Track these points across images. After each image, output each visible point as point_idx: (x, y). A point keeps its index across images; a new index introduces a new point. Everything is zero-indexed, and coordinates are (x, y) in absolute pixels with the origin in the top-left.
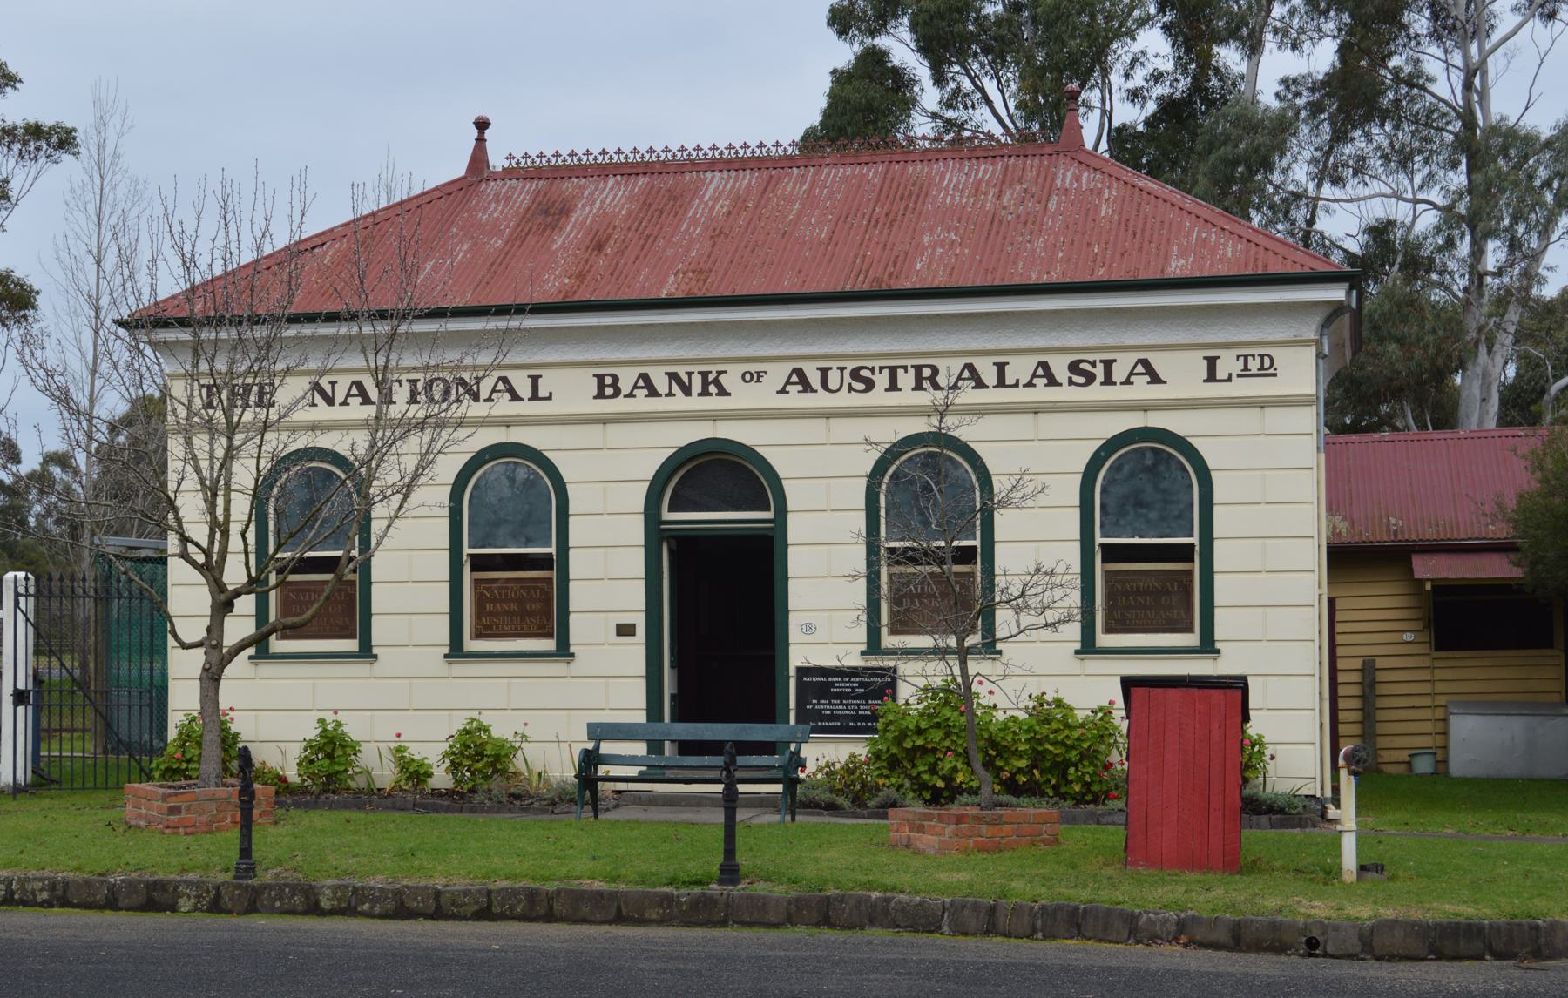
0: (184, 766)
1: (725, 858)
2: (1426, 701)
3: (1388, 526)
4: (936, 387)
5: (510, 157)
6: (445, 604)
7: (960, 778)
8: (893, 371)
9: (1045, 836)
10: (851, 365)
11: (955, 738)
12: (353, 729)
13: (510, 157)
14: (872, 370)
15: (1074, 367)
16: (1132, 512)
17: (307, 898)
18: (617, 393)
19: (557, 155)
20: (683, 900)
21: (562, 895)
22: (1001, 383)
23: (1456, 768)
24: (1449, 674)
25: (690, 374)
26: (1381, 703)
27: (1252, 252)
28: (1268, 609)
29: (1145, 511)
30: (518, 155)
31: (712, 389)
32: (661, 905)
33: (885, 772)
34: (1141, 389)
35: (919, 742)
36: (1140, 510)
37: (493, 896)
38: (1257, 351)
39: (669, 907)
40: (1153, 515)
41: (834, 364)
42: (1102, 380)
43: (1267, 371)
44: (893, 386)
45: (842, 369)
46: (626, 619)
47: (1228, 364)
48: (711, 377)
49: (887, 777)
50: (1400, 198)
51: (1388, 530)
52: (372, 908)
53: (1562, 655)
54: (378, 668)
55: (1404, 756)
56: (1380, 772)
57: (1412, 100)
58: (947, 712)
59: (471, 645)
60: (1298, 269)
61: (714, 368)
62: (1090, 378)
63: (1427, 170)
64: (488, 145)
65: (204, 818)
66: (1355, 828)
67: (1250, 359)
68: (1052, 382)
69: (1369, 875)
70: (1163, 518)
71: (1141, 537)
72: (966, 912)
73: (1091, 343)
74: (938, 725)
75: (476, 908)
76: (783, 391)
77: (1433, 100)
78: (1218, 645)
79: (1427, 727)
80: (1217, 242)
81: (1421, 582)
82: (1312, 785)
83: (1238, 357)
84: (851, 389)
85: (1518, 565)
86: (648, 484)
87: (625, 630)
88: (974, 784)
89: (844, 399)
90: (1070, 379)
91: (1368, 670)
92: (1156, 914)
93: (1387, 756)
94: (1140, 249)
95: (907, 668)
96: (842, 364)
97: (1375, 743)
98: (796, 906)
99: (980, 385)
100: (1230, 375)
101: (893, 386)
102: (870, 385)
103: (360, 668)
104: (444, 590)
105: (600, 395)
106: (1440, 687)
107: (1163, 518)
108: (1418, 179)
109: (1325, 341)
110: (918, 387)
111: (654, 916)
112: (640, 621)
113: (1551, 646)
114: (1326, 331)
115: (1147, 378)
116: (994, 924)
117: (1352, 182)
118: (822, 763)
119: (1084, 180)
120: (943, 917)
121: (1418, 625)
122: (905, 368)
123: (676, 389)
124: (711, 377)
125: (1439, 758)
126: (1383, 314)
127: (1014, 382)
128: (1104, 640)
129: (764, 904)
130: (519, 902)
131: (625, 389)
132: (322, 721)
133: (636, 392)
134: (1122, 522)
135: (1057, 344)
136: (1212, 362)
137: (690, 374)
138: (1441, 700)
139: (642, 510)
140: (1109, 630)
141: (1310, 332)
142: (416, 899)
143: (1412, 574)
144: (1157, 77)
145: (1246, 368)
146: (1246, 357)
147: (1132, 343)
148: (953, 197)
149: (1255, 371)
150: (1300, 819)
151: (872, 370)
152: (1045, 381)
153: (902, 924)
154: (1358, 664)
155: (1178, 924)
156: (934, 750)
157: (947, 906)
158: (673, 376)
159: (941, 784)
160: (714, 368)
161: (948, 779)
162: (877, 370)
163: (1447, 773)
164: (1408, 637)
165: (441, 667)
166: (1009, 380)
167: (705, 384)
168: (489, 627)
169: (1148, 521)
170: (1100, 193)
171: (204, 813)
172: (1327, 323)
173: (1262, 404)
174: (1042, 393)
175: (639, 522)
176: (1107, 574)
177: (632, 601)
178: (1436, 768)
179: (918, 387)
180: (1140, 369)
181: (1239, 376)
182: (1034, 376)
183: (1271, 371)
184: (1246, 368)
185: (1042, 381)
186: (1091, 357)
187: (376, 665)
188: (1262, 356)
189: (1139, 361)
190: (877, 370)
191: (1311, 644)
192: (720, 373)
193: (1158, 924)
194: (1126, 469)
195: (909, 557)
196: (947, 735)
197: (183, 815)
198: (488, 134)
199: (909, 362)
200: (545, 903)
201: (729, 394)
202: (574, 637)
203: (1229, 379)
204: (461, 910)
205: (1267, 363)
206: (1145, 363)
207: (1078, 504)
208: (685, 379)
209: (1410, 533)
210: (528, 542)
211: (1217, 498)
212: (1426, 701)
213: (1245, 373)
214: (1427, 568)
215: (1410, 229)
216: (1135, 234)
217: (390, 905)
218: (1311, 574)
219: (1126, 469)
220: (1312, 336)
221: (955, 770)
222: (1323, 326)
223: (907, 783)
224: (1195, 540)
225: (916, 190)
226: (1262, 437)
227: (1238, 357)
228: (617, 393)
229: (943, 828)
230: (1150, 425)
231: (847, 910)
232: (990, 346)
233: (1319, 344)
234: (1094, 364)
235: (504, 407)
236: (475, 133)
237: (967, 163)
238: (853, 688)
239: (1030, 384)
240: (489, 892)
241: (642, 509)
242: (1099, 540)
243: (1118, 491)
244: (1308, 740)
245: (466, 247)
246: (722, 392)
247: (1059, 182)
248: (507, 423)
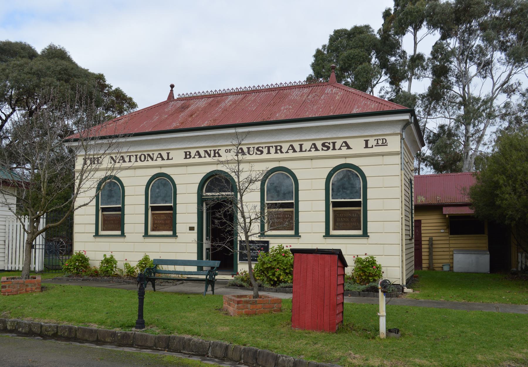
0: (70, 267)
1: (139, 318)
2: (447, 250)
3: (436, 199)
4: (282, 152)
5: (179, 95)
6: (143, 221)
7: (281, 278)
8: (269, 148)
9: (275, 308)
10: (256, 146)
11: (280, 264)
12: (116, 257)
13: (179, 95)
14: (263, 148)
15: (323, 145)
16: (341, 191)
17: (4, 325)
18: (190, 157)
19: (191, 93)
20: (119, 335)
21: (80, 330)
22: (301, 150)
23: (456, 269)
24: (454, 242)
25: (210, 151)
26: (434, 250)
27: (380, 106)
28: (385, 222)
29: (345, 191)
30: (181, 94)
31: (217, 155)
32: (111, 336)
33: (259, 275)
34: (345, 151)
35: (269, 266)
36: (344, 190)
37: (59, 328)
38: (381, 138)
39: (114, 337)
40: (348, 192)
41: (252, 146)
43: (384, 144)
44: (269, 153)
45: (254, 148)
46: (192, 225)
47: (372, 142)
48: (216, 151)
49: (259, 277)
50: (446, 118)
51: (436, 201)
52: (22, 330)
53: (487, 236)
54: (126, 239)
55: (441, 265)
56: (433, 270)
57: (448, 93)
58: (279, 256)
59: (333, 232)
60: (391, 109)
61: (217, 149)
62: (328, 148)
63: (453, 111)
64: (174, 92)
65: (15, 290)
66: (385, 315)
67: (379, 140)
68: (317, 150)
69: (393, 335)
70: (351, 193)
72: (217, 348)
73: (329, 137)
74: (275, 260)
75: (53, 332)
77: (454, 93)
78: (369, 234)
79: (448, 257)
80: (370, 104)
81: (445, 215)
82: (399, 281)
83: (375, 140)
84: (256, 154)
85: (472, 209)
86: (198, 184)
87: (192, 229)
88: (286, 280)
89: (255, 157)
90: (322, 148)
91: (431, 240)
92: (286, 357)
93: (436, 265)
94: (345, 107)
96: (254, 146)
97: (432, 262)
98: (158, 340)
99: (295, 151)
100: (373, 146)
101: (269, 153)
102: (262, 152)
103: (121, 239)
104: (143, 217)
105: (186, 158)
106: (451, 246)
107: (351, 193)
108: (451, 113)
109: (404, 134)
110: (276, 152)
111: (109, 340)
112: (196, 226)
113: (484, 234)
114: (404, 130)
115: (346, 147)
116: (227, 354)
117: (434, 115)
118: (243, 271)
119: (334, 91)
120: (209, 349)
121: (445, 228)
122: (272, 147)
123: (207, 155)
124: (216, 151)
125: (451, 266)
126: (441, 146)
127: (305, 150)
128: (101, 233)
129: (146, 339)
130: (66, 331)
131: (193, 156)
132: (105, 255)
133: (195, 157)
134: (338, 194)
135: (318, 137)
136: (367, 142)
137: (210, 151)
138: (452, 249)
139: (197, 192)
140: (335, 229)
141: (398, 131)
142: (35, 328)
143: (443, 212)
145: (378, 143)
146: (378, 140)
147: (341, 136)
148: (294, 97)
149: (380, 144)
150: (391, 294)
151: (263, 148)
152: (314, 149)
153: (194, 351)
154: (428, 239)
155: (294, 363)
156: (274, 268)
157: (211, 344)
158: (206, 151)
159: (276, 279)
160: (217, 149)
161: (278, 278)
162: (264, 148)
163: (453, 270)
164: (442, 231)
165: (141, 239)
166: (304, 149)
167: (215, 153)
168: (156, 228)
169: (346, 194)
170: (337, 93)
171: (15, 288)
172: (404, 128)
173: (383, 155)
174: (313, 153)
176: (334, 211)
177: (193, 220)
178: (450, 269)
179: (276, 152)
180: (344, 144)
181: (375, 146)
182: (311, 148)
183: (386, 144)
184: (378, 143)
185: (313, 150)
186: (328, 141)
187: (126, 238)
188: (383, 139)
189: (344, 142)
190: (264, 148)
191: (399, 234)
192: (219, 150)
193: (286, 362)
195: (275, 205)
196: (278, 264)
197: (7, 288)
198: (174, 89)
199: (273, 145)
200: (74, 333)
201: (221, 156)
202: (301, 230)
203: (372, 147)
204: (48, 333)
205: (384, 141)
206: (345, 143)
207: (324, 188)
208: (209, 152)
209: (442, 201)
210: (166, 202)
211: (368, 186)
212: (447, 250)
213: (377, 145)
214: (447, 211)
215: (450, 125)
216: (345, 103)
217: (27, 329)
218: (399, 211)
220: (399, 132)
221: (280, 275)
222: (403, 129)
223: (265, 279)
224: (361, 200)
225: (284, 96)
226: (383, 166)
227: (375, 140)
228: (190, 157)
229: (234, 305)
230: (347, 162)
231: (175, 343)
232: (298, 139)
233: (402, 135)
234: (329, 144)
235: (159, 162)
236: (170, 89)
237: (301, 89)
238: (256, 247)
239: (310, 151)
240: (57, 327)
241: (196, 192)
242: (331, 200)
244: (398, 266)
245: (157, 118)
246: (220, 156)
247: (326, 92)
248: (161, 167)
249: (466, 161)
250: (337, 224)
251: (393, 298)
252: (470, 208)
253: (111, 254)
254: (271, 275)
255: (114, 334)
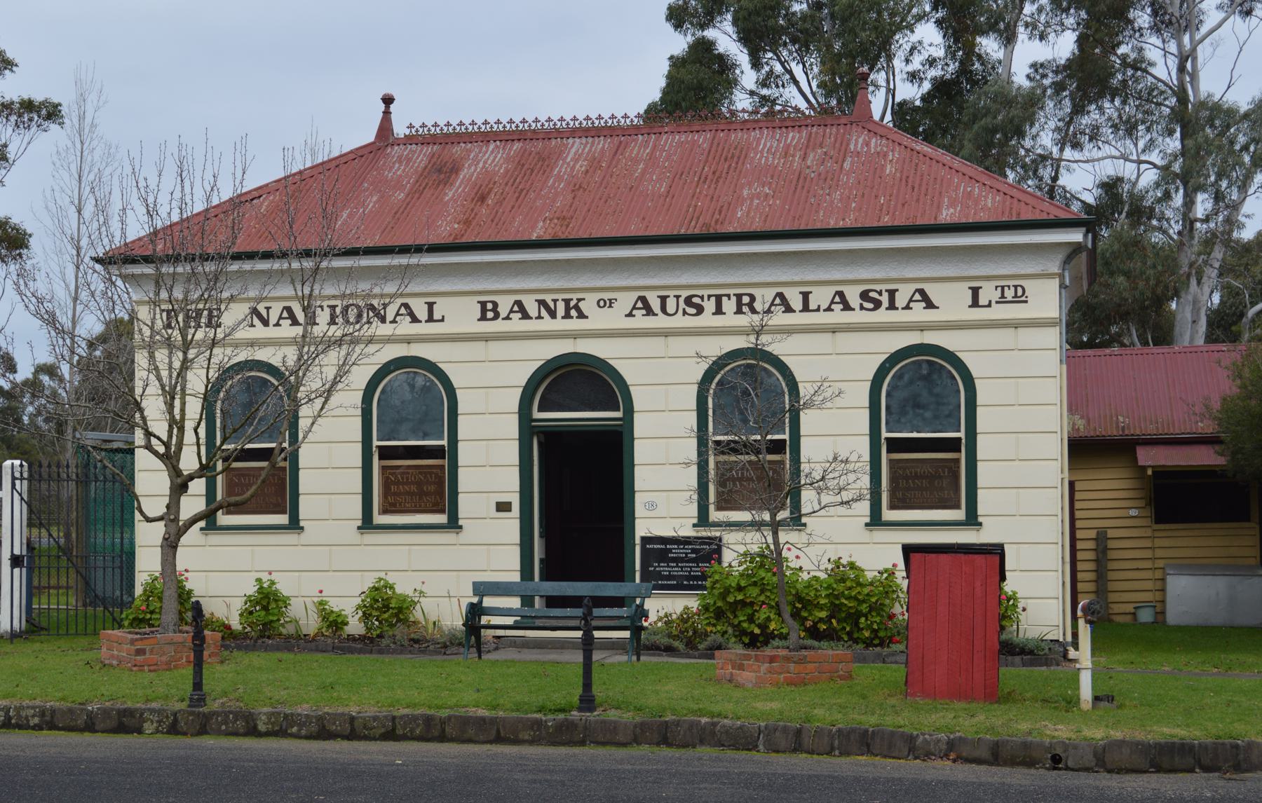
0: (148, 616)
1: (584, 691)
2: (1148, 564)
3: (1117, 423)
5: (411, 126)
6: (358, 486)
7: (772, 626)
8: (719, 299)
9: (841, 673)
10: (685, 294)
11: (768, 594)
12: (285, 587)
13: (411, 126)
14: (702, 298)
15: (865, 296)
16: (911, 412)
17: (247, 722)
18: (497, 316)
19: (448, 124)
20: (550, 724)
21: (453, 720)
22: (806, 308)
23: (1172, 618)
24: (1166, 543)
25: (555, 301)
26: (1111, 565)
27: (1008, 203)
28: (1020, 490)
29: (921, 411)
30: (417, 125)
31: (573, 313)
32: (532, 728)
33: (713, 621)
34: (919, 313)
35: (740, 597)
36: (917, 411)
37: (397, 721)
38: (1012, 283)
39: (539, 729)
40: (928, 414)
41: (672, 293)
42: (887, 306)
43: (1020, 298)
44: (719, 311)
45: (678, 297)
46: (504, 498)
47: (988, 293)
48: (572, 304)
49: (714, 625)
50: (1126, 159)
51: (1117, 427)
52: (299, 730)
54: (304, 538)
55: (1130, 608)
56: (1111, 621)
58: (762, 573)
59: (379, 519)
61: (575, 296)
62: (878, 304)
63: (1148, 137)
64: (393, 117)
65: (164, 659)
66: (1091, 666)
67: (1006, 288)
68: (847, 307)
69: (1102, 704)
70: (936, 417)
71: (918, 432)
72: (777, 734)
73: (878, 276)
74: (755, 584)
75: (383, 730)
76: (630, 315)
77: (1154, 80)
78: (980, 519)
79: (1149, 585)
80: (980, 195)
81: (1144, 468)
82: (1056, 632)
83: (997, 287)
84: (685, 313)
85: (1222, 455)
86: (521, 389)
87: (503, 507)
88: (784, 631)
89: (680, 321)
90: (861, 305)
91: (1101, 539)
92: (930, 735)
93: (1116, 608)
94: (918, 200)
95: (730, 537)
96: (677, 293)
97: (1107, 598)
98: (641, 729)
99: (789, 310)
100: (990, 301)
101: (719, 311)
102: (700, 310)
103: (290, 538)
104: (358, 475)
105: (483, 318)
106: (1159, 553)
107: (936, 417)
108: (1141, 144)
109: (1067, 274)
110: (739, 311)
111: (527, 737)
112: (515, 500)
113: (1248, 520)
114: (1067, 266)
115: (924, 304)
116: (800, 744)
117: (1088, 146)
118: (662, 614)
119: (873, 145)
120: (759, 738)
121: (1142, 503)
122: (729, 296)
123: (544, 313)
124: (572, 304)
125: (1158, 610)
126: (1113, 253)
127: (816, 307)
128: (888, 515)
129: (615, 728)
130: (418, 725)
131: (503, 313)
132: (259, 580)
133: (512, 315)
134: (903, 420)
135: (851, 277)
136: (975, 291)
137: (555, 301)
138: (1160, 564)
139: (517, 410)
140: (893, 507)
141: (1055, 268)
142: (335, 723)
143: (1137, 462)
144: (932, 62)
145: (1003, 296)
146: (1003, 287)
147: (911, 276)
148: (767, 158)
149: (1010, 299)
150: (1046, 659)
151: (702, 298)
152: (841, 306)
153: (726, 744)
154: (1093, 534)
155: (948, 743)
156: (752, 604)
157: (762, 729)
158: (542, 303)
159: (757, 631)
160: (575, 296)
161: (763, 627)
162: (706, 298)
163: (1164, 622)
164: (1133, 512)
165: (355, 536)
166: (812, 306)
167: (568, 309)
168: (393, 505)
169: (924, 419)
170: (885, 155)
171: (164, 654)
172: (1068, 260)
173: (1016, 325)
174: (838, 316)
175: (515, 420)
176: (891, 462)
177: (508, 484)
178: (1156, 618)
179: (739, 311)
180: (917, 297)
181: (997, 302)
182: (832, 302)
183: (1023, 298)
184: (1003, 296)
185: (839, 307)
186: (878, 287)
187: (303, 535)
188: (1016, 287)
189: (917, 290)
190: (706, 298)
191: (1055, 518)
192: (579, 300)
193: (932, 744)
194: (906, 377)
195: (732, 448)
196: (762, 591)
197: (148, 655)
198: (393, 108)
199: (732, 292)
200: (439, 727)
201: (587, 317)
202: (462, 513)
203: (989, 305)
204: (371, 732)
205: (1020, 292)
206: (922, 292)
207: (868, 405)
208: (552, 305)
209: (1135, 428)
210: (425, 436)
211: (979, 401)
212: (1148, 564)
213: (1002, 300)
214: (1148, 457)
215: (1135, 184)
216: (913, 188)
217: (314, 728)
218: (1055, 462)
219: (906, 377)
220: (1056, 271)
221: (768, 619)
222: (1065, 262)
224: (961, 434)
225: (737, 153)
226: (1016, 352)
227: (997, 287)
228: (497, 316)
229: (759, 667)
230: (926, 342)
231: (682, 732)
232: (797, 279)
233: (1062, 276)
234: (880, 293)
235: (406, 327)
236: (382, 107)
237: (778, 131)
238: (686, 554)
239: (829, 309)
240: (394, 718)
241: (516, 410)
242: (885, 434)
243: (900, 395)
244: (1052, 596)
245: (375, 199)
246: (581, 315)
247: (852, 147)
248: (408, 340)
249: (1186, 293)
250: (900, 495)
251: (1052, 668)
252: (1216, 452)
253: (269, 577)
254: (744, 621)
255: (538, 724)
